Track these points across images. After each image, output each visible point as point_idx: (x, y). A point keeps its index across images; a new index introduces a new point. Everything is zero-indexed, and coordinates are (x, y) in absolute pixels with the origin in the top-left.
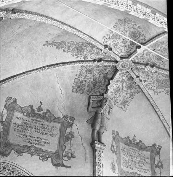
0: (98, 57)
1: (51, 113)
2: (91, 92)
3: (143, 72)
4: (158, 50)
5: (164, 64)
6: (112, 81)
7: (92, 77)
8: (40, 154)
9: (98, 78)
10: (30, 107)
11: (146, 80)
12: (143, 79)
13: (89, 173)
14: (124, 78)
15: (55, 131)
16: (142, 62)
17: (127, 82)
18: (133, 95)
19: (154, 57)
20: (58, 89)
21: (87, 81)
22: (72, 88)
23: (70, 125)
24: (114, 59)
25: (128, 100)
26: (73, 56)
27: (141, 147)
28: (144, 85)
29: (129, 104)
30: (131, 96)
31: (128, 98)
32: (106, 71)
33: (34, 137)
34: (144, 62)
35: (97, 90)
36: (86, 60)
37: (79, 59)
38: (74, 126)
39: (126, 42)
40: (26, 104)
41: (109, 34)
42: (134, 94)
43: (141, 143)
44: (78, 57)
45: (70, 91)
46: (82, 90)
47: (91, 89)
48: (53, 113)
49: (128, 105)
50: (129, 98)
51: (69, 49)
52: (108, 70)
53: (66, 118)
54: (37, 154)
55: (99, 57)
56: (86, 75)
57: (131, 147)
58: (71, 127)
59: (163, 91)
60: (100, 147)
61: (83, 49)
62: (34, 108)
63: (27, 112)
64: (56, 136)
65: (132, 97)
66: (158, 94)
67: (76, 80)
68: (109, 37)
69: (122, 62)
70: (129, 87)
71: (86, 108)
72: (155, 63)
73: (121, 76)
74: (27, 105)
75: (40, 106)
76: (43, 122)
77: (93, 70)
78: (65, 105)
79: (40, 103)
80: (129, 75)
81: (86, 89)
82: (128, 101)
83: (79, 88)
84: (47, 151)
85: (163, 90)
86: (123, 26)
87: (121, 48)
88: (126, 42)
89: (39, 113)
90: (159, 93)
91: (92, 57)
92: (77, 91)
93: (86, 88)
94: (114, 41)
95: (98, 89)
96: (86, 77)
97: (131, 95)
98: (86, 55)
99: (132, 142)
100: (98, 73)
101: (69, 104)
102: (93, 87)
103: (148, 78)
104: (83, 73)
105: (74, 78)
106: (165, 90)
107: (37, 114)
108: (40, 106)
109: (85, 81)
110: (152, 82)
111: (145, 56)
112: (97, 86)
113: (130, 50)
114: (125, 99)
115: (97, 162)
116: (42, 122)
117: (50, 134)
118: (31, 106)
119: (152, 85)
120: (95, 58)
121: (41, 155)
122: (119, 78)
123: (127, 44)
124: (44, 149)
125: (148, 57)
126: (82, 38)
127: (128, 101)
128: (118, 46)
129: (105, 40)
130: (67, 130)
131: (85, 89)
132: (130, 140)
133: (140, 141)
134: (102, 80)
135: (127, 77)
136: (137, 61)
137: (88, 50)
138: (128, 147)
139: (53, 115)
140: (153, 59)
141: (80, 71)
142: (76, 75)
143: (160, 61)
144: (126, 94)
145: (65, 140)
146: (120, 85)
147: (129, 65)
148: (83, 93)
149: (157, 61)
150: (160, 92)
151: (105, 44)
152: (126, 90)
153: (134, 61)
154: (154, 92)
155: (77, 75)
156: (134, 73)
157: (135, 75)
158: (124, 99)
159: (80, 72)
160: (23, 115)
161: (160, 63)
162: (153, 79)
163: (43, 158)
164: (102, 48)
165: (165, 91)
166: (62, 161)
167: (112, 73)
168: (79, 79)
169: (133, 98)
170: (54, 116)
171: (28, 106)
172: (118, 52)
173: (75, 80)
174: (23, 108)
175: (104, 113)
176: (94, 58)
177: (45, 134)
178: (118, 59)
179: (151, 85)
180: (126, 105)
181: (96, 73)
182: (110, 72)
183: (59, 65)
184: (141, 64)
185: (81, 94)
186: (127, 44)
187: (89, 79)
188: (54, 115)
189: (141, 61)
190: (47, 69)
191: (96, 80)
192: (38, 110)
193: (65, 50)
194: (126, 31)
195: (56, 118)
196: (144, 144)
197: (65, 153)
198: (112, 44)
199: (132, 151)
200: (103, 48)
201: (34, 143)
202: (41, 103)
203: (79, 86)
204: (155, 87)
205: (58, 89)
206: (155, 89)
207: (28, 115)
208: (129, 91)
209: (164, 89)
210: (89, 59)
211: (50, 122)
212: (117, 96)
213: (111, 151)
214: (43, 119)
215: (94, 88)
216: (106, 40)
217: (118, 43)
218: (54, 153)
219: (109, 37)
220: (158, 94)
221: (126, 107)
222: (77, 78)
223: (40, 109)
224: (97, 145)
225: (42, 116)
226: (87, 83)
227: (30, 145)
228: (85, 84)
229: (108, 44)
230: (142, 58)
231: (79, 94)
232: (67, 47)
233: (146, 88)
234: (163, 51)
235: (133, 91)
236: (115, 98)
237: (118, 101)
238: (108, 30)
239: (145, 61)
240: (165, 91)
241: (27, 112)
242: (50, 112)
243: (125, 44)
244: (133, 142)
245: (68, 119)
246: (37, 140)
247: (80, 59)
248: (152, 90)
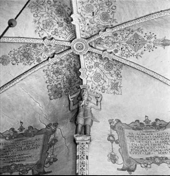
0: (50, 54)
1: (34, 128)
2: (69, 91)
3: (106, 43)
4: (97, 11)
5: (114, 20)
6: (80, 69)
7: (64, 77)
8: (20, 169)
9: (70, 74)
10: (11, 130)
11: (117, 49)
12: (112, 51)
13: (69, 171)
14: (95, 61)
15: (38, 143)
16: (94, 34)
17: (102, 65)
18: (118, 73)
19: (100, 20)
20: (34, 103)
21: (61, 83)
22: (48, 96)
23: (54, 132)
24: (66, 46)
25: (117, 81)
26: (26, 65)
27: (161, 126)
28: (119, 56)
29: (121, 86)
30: (117, 76)
31: (116, 79)
32: (73, 64)
33: (16, 156)
34: (95, 32)
35: (74, 87)
36: (40, 62)
37: (33, 65)
38: (58, 131)
39: (62, 23)
40: (6, 128)
41: (38, 26)
42: (119, 72)
43: (158, 122)
44: (31, 63)
45: (48, 100)
46: (60, 93)
47: (68, 89)
48: (35, 128)
49: (120, 87)
50: (117, 78)
51: (16, 60)
52: (73, 61)
53: (49, 127)
54: (18, 170)
55: (51, 53)
56: (57, 77)
57: (144, 130)
58: (55, 133)
59: (145, 50)
60: (82, 139)
61: (30, 54)
62: (16, 130)
63: (9, 135)
64: (38, 147)
65: (119, 76)
66: (141, 57)
67: (49, 87)
68: (42, 29)
69: (74, 45)
70: (109, 67)
71: (68, 108)
72: (106, 25)
73: (90, 60)
74: (7, 130)
75: (21, 125)
76: (26, 139)
77: (60, 69)
78: (46, 114)
79: (20, 123)
80: (97, 55)
81: (63, 91)
82: (118, 83)
83: (56, 93)
84: (28, 164)
85: (143, 49)
86: (42, 11)
87: (64, 32)
88: (62, 23)
89: (22, 132)
90: (141, 55)
91: (44, 57)
92: (55, 96)
93: (63, 90)
94: (50, 29)
95: (75, 84)
96: (58, 80)
97: (118, 75)
98: (38, 58)
99: (145, 124)
100: (67, 70)
101: (50, 112)
102: (70, 86)
103: (116, 46)
104: (52, 78)
105: (46, 86)
106: (145, 47)
107: (20, 134)
108: (21, 125)
109: (60, 84)
110: (125, 47)
111: (92, 25)
112: (72, 83)
113: (72, 29)
114: (114, 82)
115: (78, 156)
116: (25, 139)
117: (33, 147)
118: (13, 129)
119: (127, 50)
120: (48, 56)
121: (21, 170)
122: (90, 63)
123: (65, 25)
124: (24, 163)
125: (95, 24)
126: (9, 41)
127: (118, 83)
128: (58, 32)
129: (39, 33)
130: (50, 137)
131: (62, 91)
132: (141, 123)
133: (157, 120)
134: (75, 74)
135: (96, 58)
136: (89, 35)
137: (35, 52)
138: (138, 132)
139: (36, 129)
140: (101, 24)
141: (47, 77)
142: (46, 82)
143: (109, 20)
144: (111, 76)
145: (48, 147)
146: (96, 70)
147: (83, 44)
148: (61, 96)
149: (106, 22)
150: (142, 53)
151: (43, 37)
152: (108, 72)
153: (86, 38)
154: (135, 57)
155: (47, 82)
156: (97, 49)
157: (101, 50)
158: (112, 83)
159: (48, 78)
160: (5, 140)
161: (110, 22)
162: (122, 44)
163: (23, 172)
164: (41, 42)
165: (146, 49)
166: (44, 169)
167: (78, 62)
168: (51, 85)
169: (121, 77)
170: (37, 130)
171: (9, 130)
172: (63, 37)
173: (47, 88)
174: (4, 134)
175: (86, 104)
176: (47, 56)
177: (27, 149)
178: (68, 44)
179: (126, 51)
180: (119, 88)
181: (64, 71)
182: (76, 62)
183: (16, 79)
184: (93, 36)
185: (60, 98)
186: (65, 25)
187: (60, 80)
188: (37, 129)
189: (92, 33)
190: (5, 87)
191: (69, 77)
192: (20, 130)
193: (14, 63)
194: (51, 13)
195: (39, 131)
196: (163, 121)
197: (47, 160)
198: (50, 34)
199: (146, 134)
200: (42, 42)
201: (15, 161)
202: (21, 122)
203: (55, 92)
204: (131, 51)
205: (34, 103)
206: (134, 53)
207: (11, 138)
208: (112, 72)
209: (143, 47)
210: (43, 60)
211: (33, 136)
212: (101, 83)
213: (108, 141)
214: (26, 136)
215: (70, 87)
216: (41, 33)
217: (56, 29)
218: (35, 164)
219: (42, 29)
220: (141, 57)
221: (119, 90)
222: (49, 85)
223: (21, 129)
224: (77, 138)
225: (25, 135)
226: (62, 85)
227: (10, 164)
228: (60, 87)
229: (45, 35)
230: (90, 29)
231: (58, 99)
232: (13, 60)
233: (122, 57)
234: (101, 8)
235: (115, 69)
236: (99, 85)
237: (106, 87)
238: (37, 24)
239: (96, 30)
240: (146, 49)
241: (9, 135)
242: (32, 128)
243: (63, 26)
244: (147, 124)
245: (52, 126)
246: (18, 157)
247: (34, 64)
248: (131, 56)
